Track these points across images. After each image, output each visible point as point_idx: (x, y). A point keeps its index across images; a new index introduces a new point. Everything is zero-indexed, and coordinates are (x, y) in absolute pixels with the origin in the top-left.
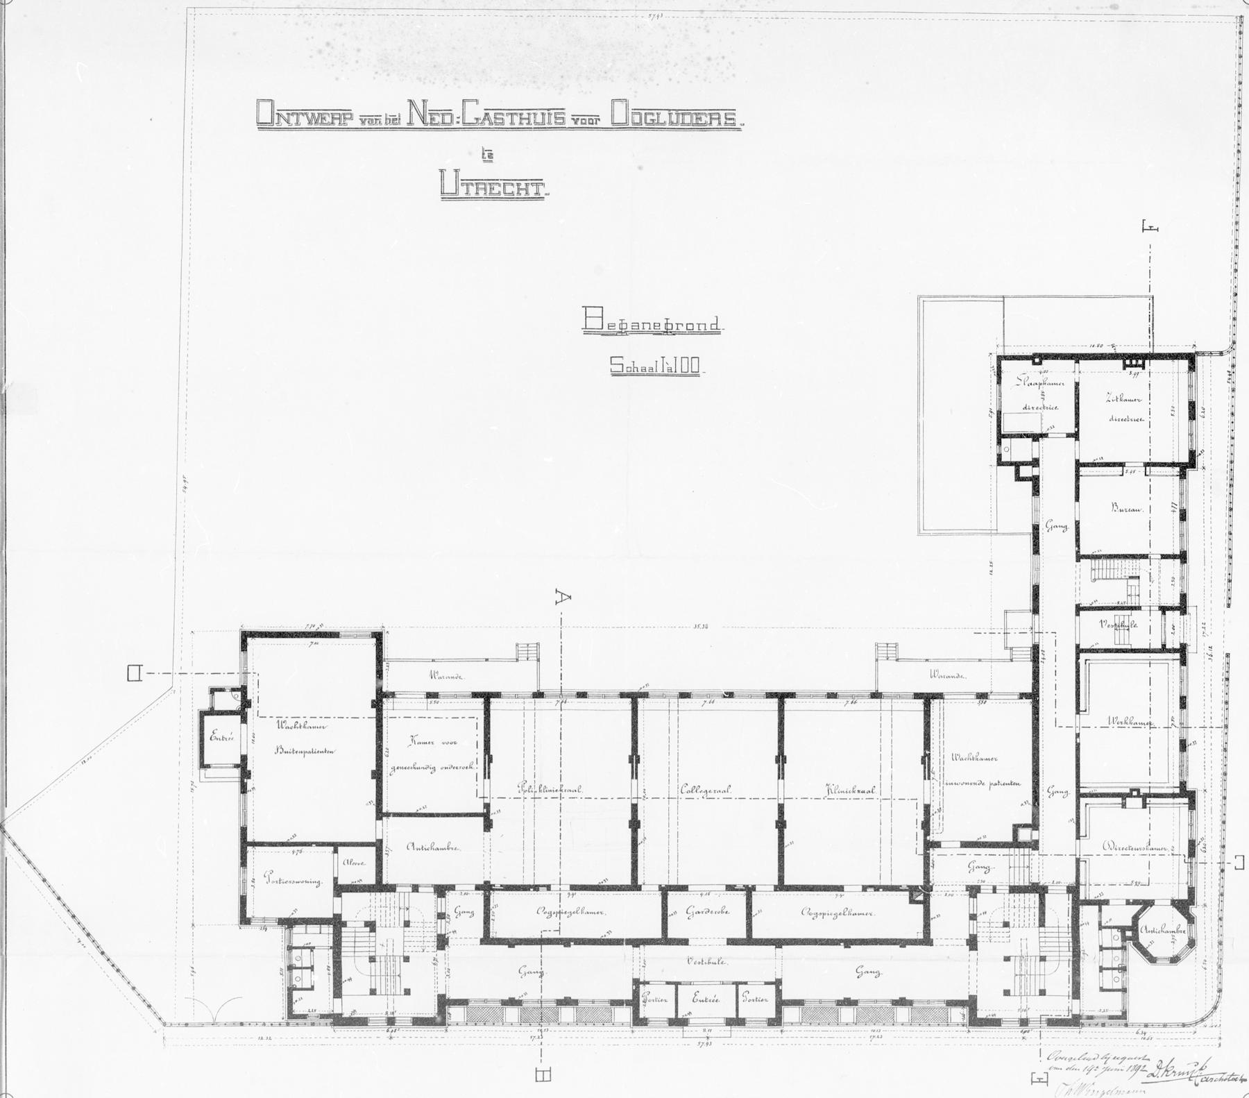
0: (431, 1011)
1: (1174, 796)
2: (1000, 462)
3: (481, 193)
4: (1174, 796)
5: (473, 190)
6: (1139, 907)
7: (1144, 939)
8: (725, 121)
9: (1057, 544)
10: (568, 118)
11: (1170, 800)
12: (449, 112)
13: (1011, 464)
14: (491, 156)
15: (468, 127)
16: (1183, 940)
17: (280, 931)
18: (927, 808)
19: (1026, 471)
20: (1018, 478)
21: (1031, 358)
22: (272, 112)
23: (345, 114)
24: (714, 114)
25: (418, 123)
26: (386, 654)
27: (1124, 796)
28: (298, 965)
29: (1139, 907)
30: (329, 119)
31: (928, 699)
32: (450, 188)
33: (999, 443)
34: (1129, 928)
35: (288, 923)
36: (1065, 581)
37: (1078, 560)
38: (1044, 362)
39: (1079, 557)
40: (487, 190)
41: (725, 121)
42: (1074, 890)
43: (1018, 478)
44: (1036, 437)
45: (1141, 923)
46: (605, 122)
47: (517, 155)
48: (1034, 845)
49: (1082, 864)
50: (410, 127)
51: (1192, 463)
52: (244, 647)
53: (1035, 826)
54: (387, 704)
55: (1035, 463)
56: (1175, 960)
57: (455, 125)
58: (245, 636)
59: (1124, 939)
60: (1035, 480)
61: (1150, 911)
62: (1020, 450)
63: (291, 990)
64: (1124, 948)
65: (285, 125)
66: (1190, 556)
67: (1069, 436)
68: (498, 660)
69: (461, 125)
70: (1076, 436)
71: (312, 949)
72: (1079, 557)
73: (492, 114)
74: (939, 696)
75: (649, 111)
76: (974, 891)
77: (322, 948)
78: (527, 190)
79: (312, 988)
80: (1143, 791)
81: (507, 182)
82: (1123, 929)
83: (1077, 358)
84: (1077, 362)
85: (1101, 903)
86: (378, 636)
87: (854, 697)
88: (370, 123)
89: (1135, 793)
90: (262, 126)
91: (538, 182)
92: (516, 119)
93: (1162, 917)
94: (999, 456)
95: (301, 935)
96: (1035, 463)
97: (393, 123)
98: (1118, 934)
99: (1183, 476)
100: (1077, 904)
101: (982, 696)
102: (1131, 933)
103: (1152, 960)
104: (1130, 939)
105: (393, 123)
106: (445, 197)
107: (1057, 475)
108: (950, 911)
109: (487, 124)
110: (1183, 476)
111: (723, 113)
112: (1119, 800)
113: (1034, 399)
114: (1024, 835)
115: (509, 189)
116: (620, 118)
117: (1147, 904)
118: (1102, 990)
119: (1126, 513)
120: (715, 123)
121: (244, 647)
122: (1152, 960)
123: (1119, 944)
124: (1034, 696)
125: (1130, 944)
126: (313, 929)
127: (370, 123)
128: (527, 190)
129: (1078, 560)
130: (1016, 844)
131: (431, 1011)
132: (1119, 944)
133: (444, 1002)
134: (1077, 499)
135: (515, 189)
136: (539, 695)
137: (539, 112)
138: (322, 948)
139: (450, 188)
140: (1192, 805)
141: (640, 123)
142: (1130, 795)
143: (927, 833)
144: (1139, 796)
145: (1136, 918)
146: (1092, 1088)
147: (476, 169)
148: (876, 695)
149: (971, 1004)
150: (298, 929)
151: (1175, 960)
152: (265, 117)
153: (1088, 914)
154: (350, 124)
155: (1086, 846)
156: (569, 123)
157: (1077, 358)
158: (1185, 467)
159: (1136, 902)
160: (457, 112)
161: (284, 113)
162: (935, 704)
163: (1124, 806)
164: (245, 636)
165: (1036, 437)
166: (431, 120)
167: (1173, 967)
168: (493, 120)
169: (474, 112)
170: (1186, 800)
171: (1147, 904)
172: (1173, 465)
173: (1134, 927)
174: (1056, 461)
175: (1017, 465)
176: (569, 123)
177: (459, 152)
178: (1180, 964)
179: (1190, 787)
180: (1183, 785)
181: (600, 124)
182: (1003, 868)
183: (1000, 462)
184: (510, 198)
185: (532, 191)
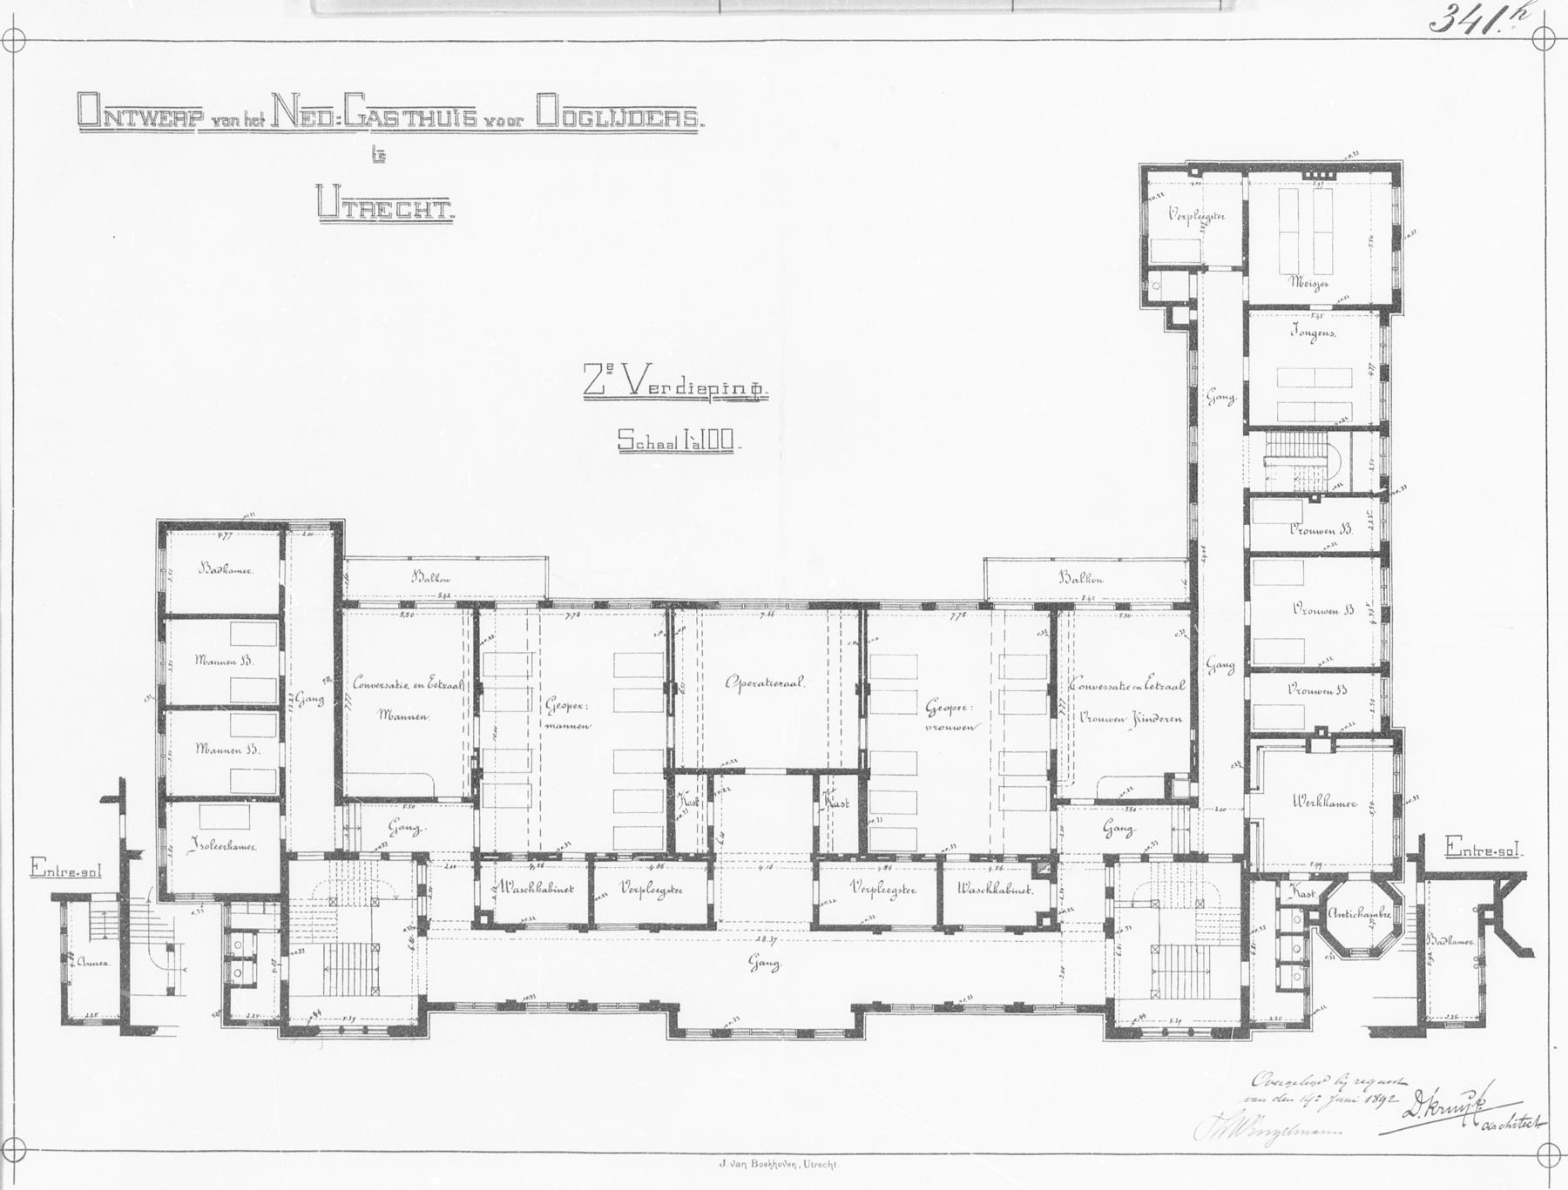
0: (409, 1016)
1: (1371, 735)
2: (1146, 302)
3: (368, 215)
4: (1371, 735)
5: (356, 212)
6: (1329, 883)
7: (1333, 925)
8: (674, 120)
9: (1220, 420)
10: (480, 117)
11: (1368, 742)
12: (328, 109)
13: (1161, 304)
14: (382, 155)
15: (351, 129)
16: (1386, 926)
17: (218, 907)
18: (1054, 753)
19: (1181, 316)
20: (1170, 326)
21: (1188, 168)
22: (98, 111)
23: (198, 114)
24: (670, 113)
25: (285, 123)
26: (349, 550)
27: (1309, 737)
28: (238, 953)
29: (1329, 883)
30: (170, 118)
31: (1054, 609)
32: (329, 209)
33: (1145, 278)
34: (1315, 908)
35: (226, 899)
36: (1230, 461)
37: (1246, 433)
38: (1205, 175)
39: (1248, 429)
40: (376, 211)
41: (674, 120)
42: (1242, 858)
43: (1170, 326)
44: (1193, 270)
45: (1330, 904)
46: (529, 123)
47: (416, 165)
48: (1193, 802)
49: (1253, 827)
50: (276, 129)
51: (1396, 306)
52: (162, 544)
53: (1194, 776)
54: (349, 615)
55: (1192, 304)
56: (1376, 952)
57: (336, 127)
58: (165, 528)
59: (1308, 922)
60: (1192, 328)
61: (1343, 889)
62: (1170, 287)
63: (228, 988)
64: (1306, 935)
65: (113, 125)
66: (1395, 429)
67: (1235, 269)
68: (493, 559)
69: (343, 126)
70: (1245, 269)
71: (255, 932)
72: (1248, 429)
73: (381, 113)
74: (1070, 606)
75: (586, 110)
76: (1111, 860)
77: (267, 931)
78: (430, 212)
79: (254, 986)
80: (1331, 730)
81: (402, 201)
82: (1307, 909)
83: (1245, 169)
84: (1245, 175)
85: (1278, 878)
86: (338, 528)
87: (958, 606)
88: (225, 125)
89: (1321, 733)
90: (85, 128)
91: (443, 202)
92: (417, 119)
93: (1358, 895)
94: (1145, 294)
95: (241, 915)
96: (1192, 304)
97: (254, 125)
98: (1299, 913)
99: (1385, 322)
100: (1248, 878)
101: (1123, 607)
102: (1317, 917)
103: (1345, 953)
104: (1314, 922)
105: (254, 125)
106: (327, 220)
107: (1219, 326)
108: (1080, 889)
109: (375, 125)
110: (1385, 322)
111: (682, 111)
112: (1303, 742)
113: (1193, 220)
114: (1181, 790)
115: (404, 210)
116: (548, 117)
117: (1339, 879)
118: (1279, 989)
119: (1316, 370)
120: (673, 124)
121: (162, 544)
122: (1345, 953)
123: (1300, 928)
124: (1192, 606)
125: (1315, 931)
126: (256, 907)
127: (225, 125)
128: (430, 212)
129: (1246, 433)
130: (1168, 799)
131: (409, 1016)
132: (1300, 928)
133: (426, 1006)
134: (1246, 353)
135: (412, 209)
136: (546, 604)
137: (444, 111)
138: (267, 931)
139: (329, 209)
140: (1398, 748)
141: (449, 124)
142: (1315, 735)
143: (1053, 790)
144: (1325, 737)
145: (1324, 898)
146: (1258, 1127)
147: (367, 182)
148: (986, 605)
149: (1108, 1008)
150: (237, 907)
151: (1376, 952)
152: (89, 116)
153: (1261, 890)
154: (199, 125)
155: (1257, 806)
156: (482, 125)
157: (1245, 169)
158: (1387, 313)
159: (1323, 877)
160: (338, 111)
161: (114, 112)
162: (1063, 617)
163: (1308, 749)
164: (165, 528)
165: (1193, 270)
166: (309, 120)
167: (1372, 964)
168: (385, 120)
169: (357, 108)
170: (1390, 742)
171: (1339, 879)
172: (1370, 307)
173: (1322, 908)
174: (1219, 303)
175: (1169, 306)
176: (482, 125)
177: (346, 162)
178: (1385, 957)
179: (1396, 723)
180: (1386, 720)
181: (524, 125)
182: (1155, 828)
183: (1146, 302)
184: (405, 220)
185: (435, 212)
